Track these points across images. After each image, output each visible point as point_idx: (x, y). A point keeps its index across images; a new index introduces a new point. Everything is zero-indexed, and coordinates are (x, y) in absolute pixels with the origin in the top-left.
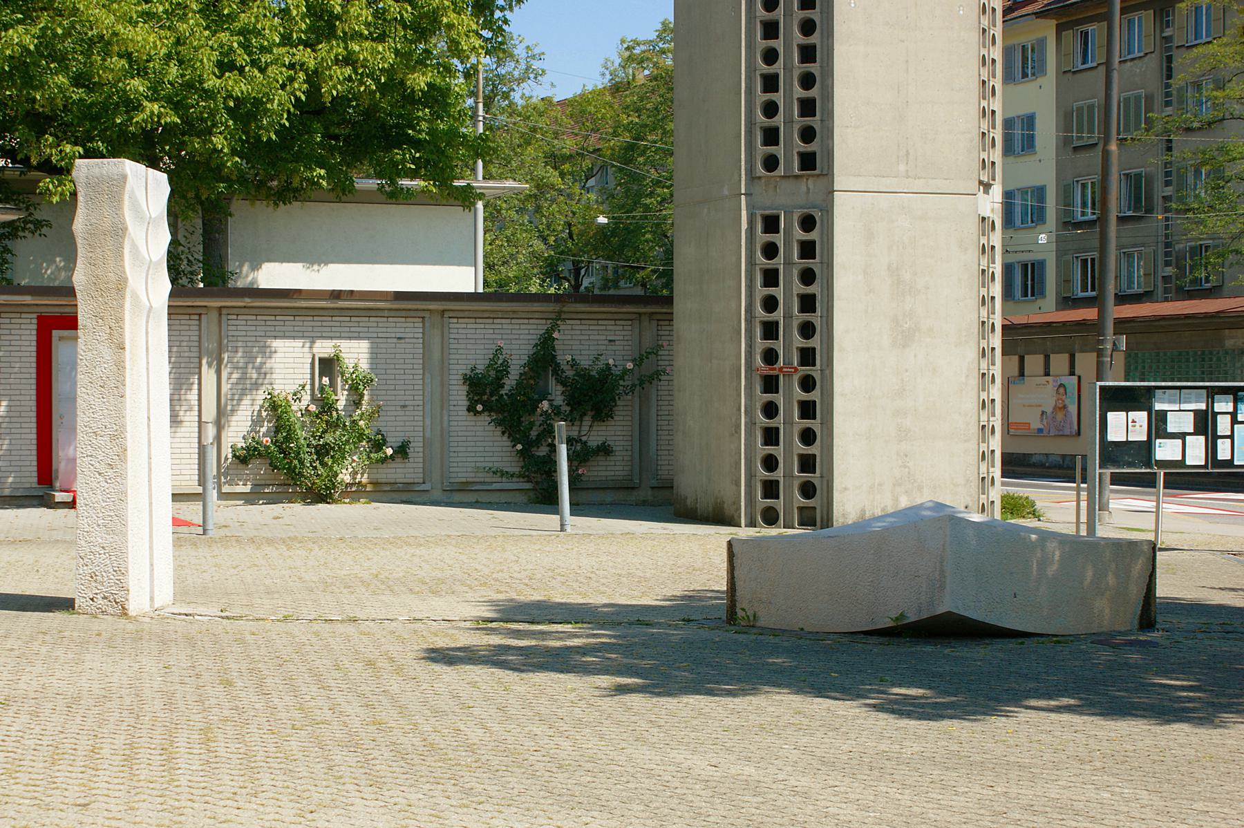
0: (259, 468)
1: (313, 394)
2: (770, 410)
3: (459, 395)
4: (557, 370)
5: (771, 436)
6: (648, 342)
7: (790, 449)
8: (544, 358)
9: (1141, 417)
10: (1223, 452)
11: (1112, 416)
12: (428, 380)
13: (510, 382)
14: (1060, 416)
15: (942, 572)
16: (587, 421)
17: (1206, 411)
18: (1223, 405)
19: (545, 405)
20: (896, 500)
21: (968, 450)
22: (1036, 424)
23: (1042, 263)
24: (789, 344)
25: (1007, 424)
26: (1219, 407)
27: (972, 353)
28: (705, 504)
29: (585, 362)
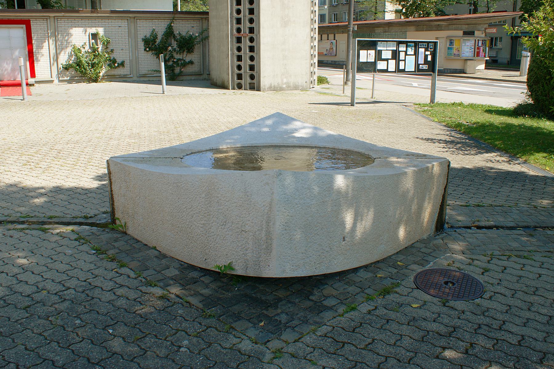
0: (72, 72)
1: (90, 46)
2: (239, 49)
3: (141, 45)
4: (174, 37)
5: (239, 58)
6: (205, 27)
7: (246, 63)
8: (169, 33)
9: (372, 52)
10: (402, 67)
11: (362, 52)
12: (130, 40)
13: (158, 41)
14: (331, 50)
15: (269, 234)
16: (185, 53)
17: (396, 50)
18: (402, 48)
19: (170, 48)
20: (282, 80)
21: (308, 62)
22: (325, 53)
23: (325, 15)
24: (245, 26)
25: (319, 54)
26: (400, 49)
27: (308, 30)
28: (219, 82)
29: (184, 34)
